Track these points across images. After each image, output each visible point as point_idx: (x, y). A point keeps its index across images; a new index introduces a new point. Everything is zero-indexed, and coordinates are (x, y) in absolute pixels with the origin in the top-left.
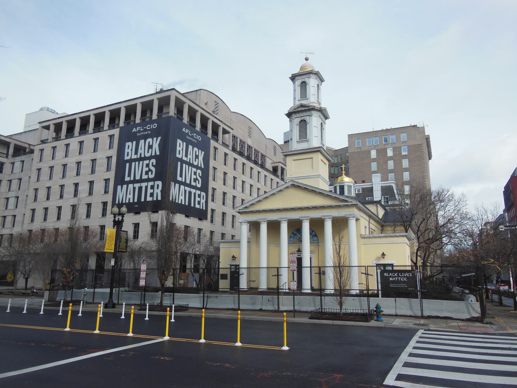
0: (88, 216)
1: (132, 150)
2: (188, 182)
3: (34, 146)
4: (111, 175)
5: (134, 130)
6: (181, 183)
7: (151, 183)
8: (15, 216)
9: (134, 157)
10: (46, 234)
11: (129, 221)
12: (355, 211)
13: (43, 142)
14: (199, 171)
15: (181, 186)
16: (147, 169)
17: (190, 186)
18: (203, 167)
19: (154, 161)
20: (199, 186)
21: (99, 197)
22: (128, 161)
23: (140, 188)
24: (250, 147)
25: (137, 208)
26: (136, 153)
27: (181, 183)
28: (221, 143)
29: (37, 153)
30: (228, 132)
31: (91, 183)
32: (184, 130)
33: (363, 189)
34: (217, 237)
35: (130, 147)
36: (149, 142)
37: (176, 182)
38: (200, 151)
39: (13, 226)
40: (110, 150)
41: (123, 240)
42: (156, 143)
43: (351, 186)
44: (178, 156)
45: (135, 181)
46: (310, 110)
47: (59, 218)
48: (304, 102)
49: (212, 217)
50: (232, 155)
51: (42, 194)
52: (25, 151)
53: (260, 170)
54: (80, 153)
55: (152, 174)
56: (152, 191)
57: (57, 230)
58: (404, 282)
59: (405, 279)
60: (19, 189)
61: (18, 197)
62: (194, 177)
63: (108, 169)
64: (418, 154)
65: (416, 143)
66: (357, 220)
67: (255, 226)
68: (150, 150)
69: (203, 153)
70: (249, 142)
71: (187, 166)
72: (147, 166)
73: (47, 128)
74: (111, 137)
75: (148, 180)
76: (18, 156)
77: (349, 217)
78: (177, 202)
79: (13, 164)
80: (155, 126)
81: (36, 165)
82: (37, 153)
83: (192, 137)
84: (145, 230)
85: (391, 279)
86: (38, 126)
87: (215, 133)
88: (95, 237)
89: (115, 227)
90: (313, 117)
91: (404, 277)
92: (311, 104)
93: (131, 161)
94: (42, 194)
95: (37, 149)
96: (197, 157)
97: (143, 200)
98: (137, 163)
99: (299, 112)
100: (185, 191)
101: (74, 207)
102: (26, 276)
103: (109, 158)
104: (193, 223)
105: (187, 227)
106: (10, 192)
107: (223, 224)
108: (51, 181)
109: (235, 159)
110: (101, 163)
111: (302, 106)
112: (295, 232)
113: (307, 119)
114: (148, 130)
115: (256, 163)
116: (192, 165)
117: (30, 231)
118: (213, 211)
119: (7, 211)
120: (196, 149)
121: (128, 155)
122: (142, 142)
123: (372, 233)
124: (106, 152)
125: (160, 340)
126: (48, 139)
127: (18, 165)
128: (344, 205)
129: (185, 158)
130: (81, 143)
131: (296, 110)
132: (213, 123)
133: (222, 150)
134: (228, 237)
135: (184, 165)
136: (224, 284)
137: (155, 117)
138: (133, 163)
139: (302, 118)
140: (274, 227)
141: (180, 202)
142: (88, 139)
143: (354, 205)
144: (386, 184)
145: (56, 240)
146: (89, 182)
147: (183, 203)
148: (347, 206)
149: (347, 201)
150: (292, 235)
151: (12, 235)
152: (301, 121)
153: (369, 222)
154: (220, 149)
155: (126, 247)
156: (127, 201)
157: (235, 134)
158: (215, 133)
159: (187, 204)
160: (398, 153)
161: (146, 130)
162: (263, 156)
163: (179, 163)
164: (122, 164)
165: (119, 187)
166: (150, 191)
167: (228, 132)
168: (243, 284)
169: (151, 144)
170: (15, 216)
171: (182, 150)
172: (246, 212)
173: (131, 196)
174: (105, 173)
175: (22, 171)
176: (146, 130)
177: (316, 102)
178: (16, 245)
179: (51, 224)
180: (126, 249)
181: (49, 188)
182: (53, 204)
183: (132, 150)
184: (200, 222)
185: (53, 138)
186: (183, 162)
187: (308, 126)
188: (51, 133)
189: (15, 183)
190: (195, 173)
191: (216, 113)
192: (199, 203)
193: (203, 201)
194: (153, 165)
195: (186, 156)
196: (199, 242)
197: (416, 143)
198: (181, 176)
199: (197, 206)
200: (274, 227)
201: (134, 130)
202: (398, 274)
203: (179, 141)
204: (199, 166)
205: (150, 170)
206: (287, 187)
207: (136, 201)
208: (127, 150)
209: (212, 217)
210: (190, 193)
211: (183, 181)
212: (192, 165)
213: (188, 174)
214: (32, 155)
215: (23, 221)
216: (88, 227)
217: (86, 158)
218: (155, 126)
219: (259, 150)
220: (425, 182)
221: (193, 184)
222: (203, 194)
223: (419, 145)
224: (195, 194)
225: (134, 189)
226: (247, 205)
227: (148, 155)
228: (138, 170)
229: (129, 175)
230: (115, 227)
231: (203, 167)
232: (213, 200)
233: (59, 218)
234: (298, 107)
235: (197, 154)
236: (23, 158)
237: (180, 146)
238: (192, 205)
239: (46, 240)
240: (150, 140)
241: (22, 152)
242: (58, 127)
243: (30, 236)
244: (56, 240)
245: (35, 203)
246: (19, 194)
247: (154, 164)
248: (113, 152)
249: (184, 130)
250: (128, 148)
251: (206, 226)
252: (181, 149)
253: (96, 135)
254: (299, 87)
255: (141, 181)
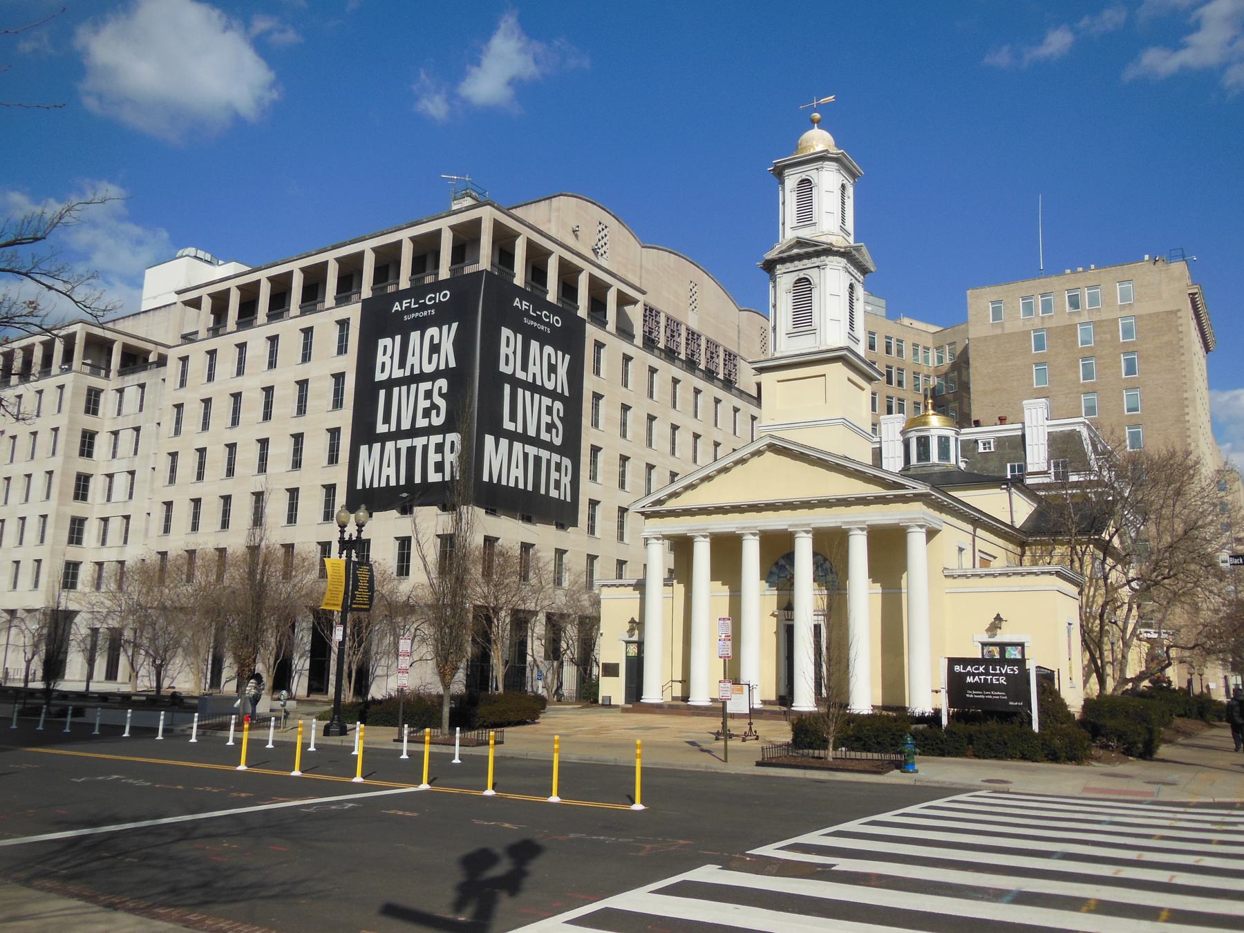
0: (292, 518)
1: (392, 357)
2: (532, 432)
3: (170, 347)
4: (344, 419)
5: (397, 307)
6: (513, 437)
7: (436, 439)
8: (127, 518)
9: (398, 373)
10: (199, 562)
11: (383, 530)
12: (918, 510)
13: (188, 338)
14: (558, 405)
15: (515, 443)
16: (427, 404)
17: (536, 442)
18: (567, 393)
19: (443, 383)
20: (558, 441)
21: (319, 472)
22: (382, 384)
23: (411, 451)
24: (693, 334)
25: (404, 498)
26: (402, 365)
27: (513, 437)
28: (614, 331)
29: (173, 366)
30: (634, 302)
31: (298, 438)
32: (517, 303)
33: (1000, 442)
34: (604, 571)
35: (387, 347)
36: (432, 337)
37: (499, 433)
38: (560, 353)
39: (125, 542)
40: (341, 357)
41: (363, 583)
42: (446, 336)
43: (947, 439)
44: (503, 368)
45: (399, 434)
46: (818, 254)
47: (225, 524)
48: (806, 233)
49: (592, 518)
50: (643, 359)
51: (187, 464)
52: (146, 360)
53: (721, 394)
54: (272, 364)
55: (438, 415)
56: (438, 458)
57: (222, 551)
58: (999, 687)
59: (1003, 681)
60: (136, 453)
61: (132, 473)
62: (546, 419)
63: (338, 403)
64: (1166, 338)
65: (1162, 309)
66: (931, 534)
67: (682, 547)
68: (435, 356)
69: (567, 357)
70: (692, 321)
71: (528, 394)
72: (428, 395)
73: (195, 304)
74: (343, 324)
75: (430, 431)
76: (133, 372)
77: (908, 527)
78: (504, 482)
79: (121, 391)
80: (445, 296)
81: (172, 394)
82: (173, 366)
83: (538, 319)
84: (427, 552)
85: (969, 679)
86: (175, 298)
87: (598, 305)
88: (307, 571)
89: (344, 555)
90: (828, 270)
91: (1001, 674)
92: (823, 239)
93: (390, 384)
94: (187, 464)
95: (173, 355)
96: (552, 369)
97: (418, 480)
98: (404, 388)
99: (791, 259)
100: (526, 455)
101: (259, 496)
102: (158, 662)
103: (339, 378)
104: (544, 537)
105: (526, 547)
106: (115, 461)
107: (621, 537)
108: (206, 433)
109: (653, 371)
110: (321, 391)
111: (800, 243)
112: (782, 562)
113: (813, 275)
114: (430, 307)
115: (710, 375)
116: (542, 391)
117: (163, 554)
118: (593, 503)
119: (109, 505)
120: (548, 349)
121: (383, 371)
122: (415, 336)
123: (985, 563)
124: (333, 362)
125: (412, 789)
126: (196, 333)
127: (132, 394)
128: (895, 496)
129: (520, 375)
130: (273, 340)
131: (785, 255)
132: (592, 279)
133: (615, 348)
134: (631, 575)
135: (520, 391)
136: (613, 689)
137: (444, 273)
138: (396, 390)
139: (801, 275)
140: (726, 551)
141: (512, 484)
142: (289, 329)
143: (921, 495)
144: (1064, 425)
145: (220, 577)
146: (292, 436)
147: (521, 486)
148: (904, 499)
149: (903, 487)
150: (775, 569)
151: (122, 563)
152: (799, 280)
153: (974, 536)
154: (607, 345)
155: (371, 598)
156: (383, 484)
157: (653, 303)
158: (598, 305)
159: (530, 488)
160: (1108, 336)
161: (424, 307)
162: (730, 357)
163: (507, 388)
164: (368, 389)
165: (364, 449)
166: (433, 458)
167: (634, 302)
168: (653, 693)
169: (436, 341)
170: (127, 518)
171: (514, 353)
172: (658, 512)
173: (391, 471)
174: (329, 416)
175: (141, 410)
176: (424, 307)
177: (837, 230)
178: (134, 588)
179: (208, 538)
180: (370, 605)
181: (202, 451)
182: (212, 488)
183: (392, 357)
184: (561, 533)
185: (208, 330)
186: (516, 383)
187: (815, 293)
188: (205, 318)
189: (126, 438)
190: (549, 411)
191: (601, 251)
192: (558, 484)
193: (566, 480)
194: (441, 395)
195: (525, 368)
196: (558, 582)
197: (1159, 307)
198: (513, 418)
199: (554, 493)
200: (726, 551)
201: (397, 307)
202: (986, 669)
203: (506, 332)
204: (559, 390)
205: (434, 406)
206: (759, 453)
207: (402, 482)
208: (380, 358)
209: (592, 518)
210: (538, 459)
211: (520, 430)
212: (542, 391)
213: (532, 413)
214: (162, 369)
215: (147, 530)
216: (292, 545)
217: (284, 379)
218: (444, 296)
219: (719, 341)
220: (1187, 418)
221: (545, 436)
222: (566, 462)
223: (1171, 312)
224: (549, 461)
225: (398, 451)
226: (661, 495)
227: (429, 369)
228: (407, 407)
229: (387, 420)
230: (344, 555)
231: (567, 393)
232: (593, 477)
233: (225, 524)
234: (791, 248)
235: (553, 362)
236: (142, 377)
237: (509, 342)
238: (543, 491)
239: (199, 576)
240: (433, 331)
241: (140, 361)
242: (220, 303)
243: (162, 569)
244: (220, 577)
245: (172, 488)
246: (136, 465)
247: (444, 390)
248: (348, 364)
249: (517, 303)
250: (384, 354)
251: (574, 540)
252: (510, 351)
253: (307, 321)
254: (795, 195)
255: (414, 432)
